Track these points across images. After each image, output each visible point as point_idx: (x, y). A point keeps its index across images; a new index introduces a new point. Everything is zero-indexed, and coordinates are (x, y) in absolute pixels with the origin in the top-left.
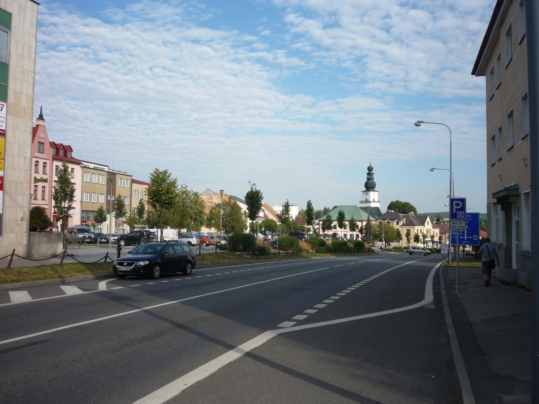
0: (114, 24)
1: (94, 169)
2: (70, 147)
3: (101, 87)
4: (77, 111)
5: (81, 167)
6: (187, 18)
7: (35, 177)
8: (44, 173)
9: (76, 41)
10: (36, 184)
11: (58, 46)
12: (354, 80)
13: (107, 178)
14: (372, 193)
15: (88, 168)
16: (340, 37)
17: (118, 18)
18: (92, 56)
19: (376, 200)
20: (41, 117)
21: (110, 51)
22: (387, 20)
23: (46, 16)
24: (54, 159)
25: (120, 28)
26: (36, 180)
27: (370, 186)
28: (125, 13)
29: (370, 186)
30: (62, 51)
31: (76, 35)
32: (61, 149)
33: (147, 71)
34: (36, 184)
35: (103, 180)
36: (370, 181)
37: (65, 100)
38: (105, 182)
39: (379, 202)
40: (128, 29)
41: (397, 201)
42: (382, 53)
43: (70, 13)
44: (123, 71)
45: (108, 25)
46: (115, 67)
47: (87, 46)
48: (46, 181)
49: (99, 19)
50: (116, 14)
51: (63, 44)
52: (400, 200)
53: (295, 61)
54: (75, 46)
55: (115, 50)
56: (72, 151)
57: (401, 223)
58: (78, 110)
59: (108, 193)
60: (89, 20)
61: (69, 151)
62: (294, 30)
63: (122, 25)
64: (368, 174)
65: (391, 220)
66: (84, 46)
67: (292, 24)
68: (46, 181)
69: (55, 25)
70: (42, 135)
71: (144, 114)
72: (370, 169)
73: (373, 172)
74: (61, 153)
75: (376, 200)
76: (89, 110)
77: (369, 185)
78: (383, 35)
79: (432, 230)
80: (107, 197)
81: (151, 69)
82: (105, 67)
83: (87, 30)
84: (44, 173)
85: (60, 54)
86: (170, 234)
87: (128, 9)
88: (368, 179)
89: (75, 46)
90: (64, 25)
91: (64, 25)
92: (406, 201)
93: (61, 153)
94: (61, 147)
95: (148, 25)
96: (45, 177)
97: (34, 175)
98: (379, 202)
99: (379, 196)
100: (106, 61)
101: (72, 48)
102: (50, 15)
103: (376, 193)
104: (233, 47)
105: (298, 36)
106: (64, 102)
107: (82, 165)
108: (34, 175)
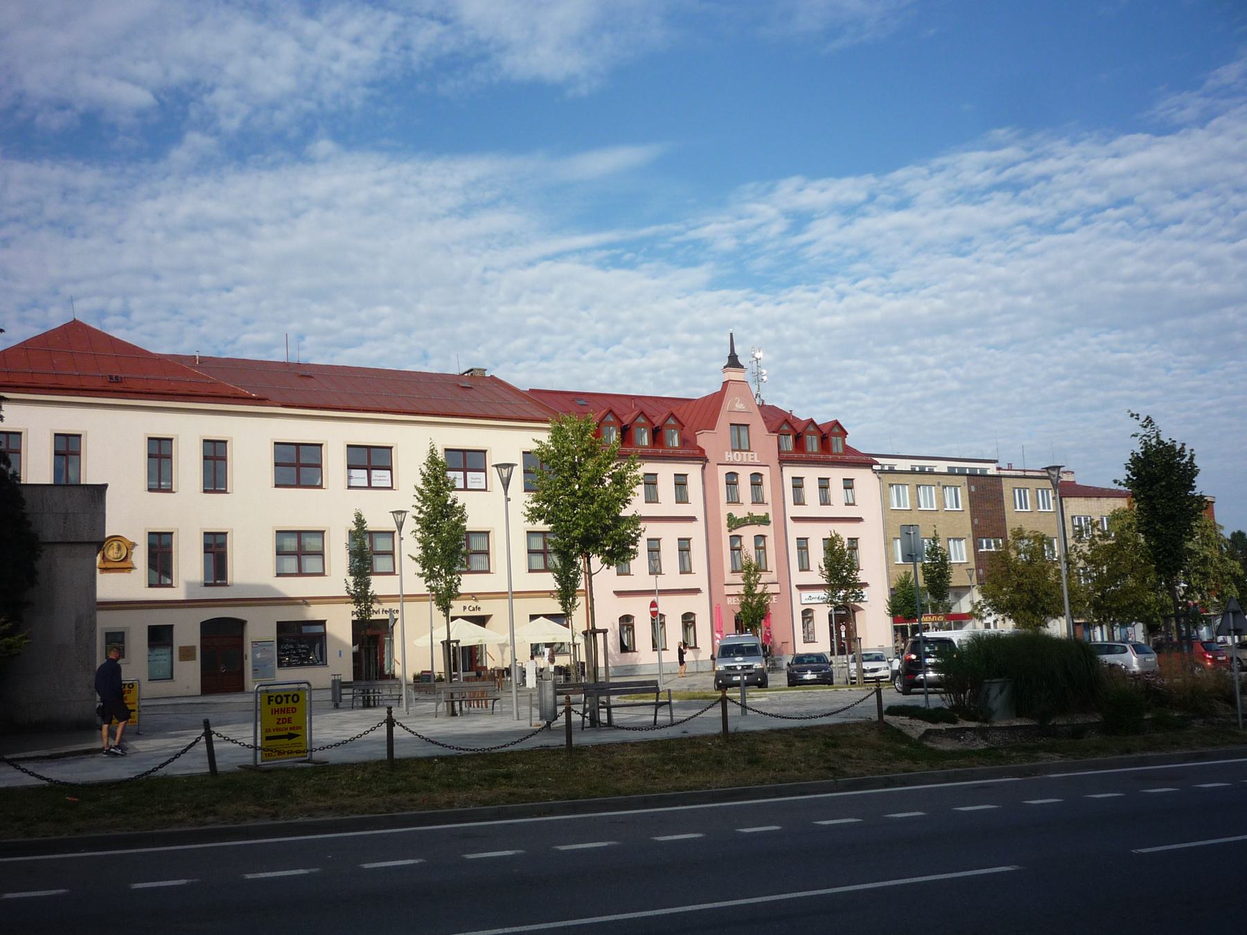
0: (1182, 132)
1: (913, 472)
2: (837, 423)
3: (1176, 285)
4: (1125, 355)
5: (875, 471)
7: (730, 515)
8: (758, 500)
9: (1098, 198)
10: (735, 532)
11: (1062, 221)
13: (970, 493)
15: (931, 473)
17: (1190, 113)
18: (1142, 221)
20: (733, 362)
21: (1185, 196)
23: (1024, 165)
24: (784, 460)
25: (1199, 135)
26: (734, 523)
28: (1206, 96)
30: (1071, 230)
32: (811, 434)
34: (735, 532)
35: (957, 500)
37: (1095, 336)
38: (964, 503)
40: (1220, 131)
43: (1074, 142)
44: (1225, 233)
45: (1168, 138)
46: (1202, 230)
47: (1128, 201)
48: (764, 521)
49: (1145, 130)
50: (1182, 107)
51: (1073, 213)
54: (1100, 209)
55: (1197, 190)
56: (844, 433)
58: (1129, 351)
59: (978, 534)
60: (1122, 142)
61: (836, 435)
63: (1202, 127)
66: (1118, 204)
68: (764, 521)
69: (1046, 178)
70: (739, 406)
74: (813, 444)
76: (1155, 346)
80: (977, 546)
82: (1180, 238)
84: (758, 500)
85: (1069, 236)
86: (758, 665)
89: (1100, 209)
90: (1067, 171)
91: (1067, 171)
93: (813, 444)
94: (811, 429)
96: (759, 511)
97: (725, 509)
101: (1094, 217)
102: (1035, 158)
106: (1093, 340)
107: (875, 467)
108: (725, 509)
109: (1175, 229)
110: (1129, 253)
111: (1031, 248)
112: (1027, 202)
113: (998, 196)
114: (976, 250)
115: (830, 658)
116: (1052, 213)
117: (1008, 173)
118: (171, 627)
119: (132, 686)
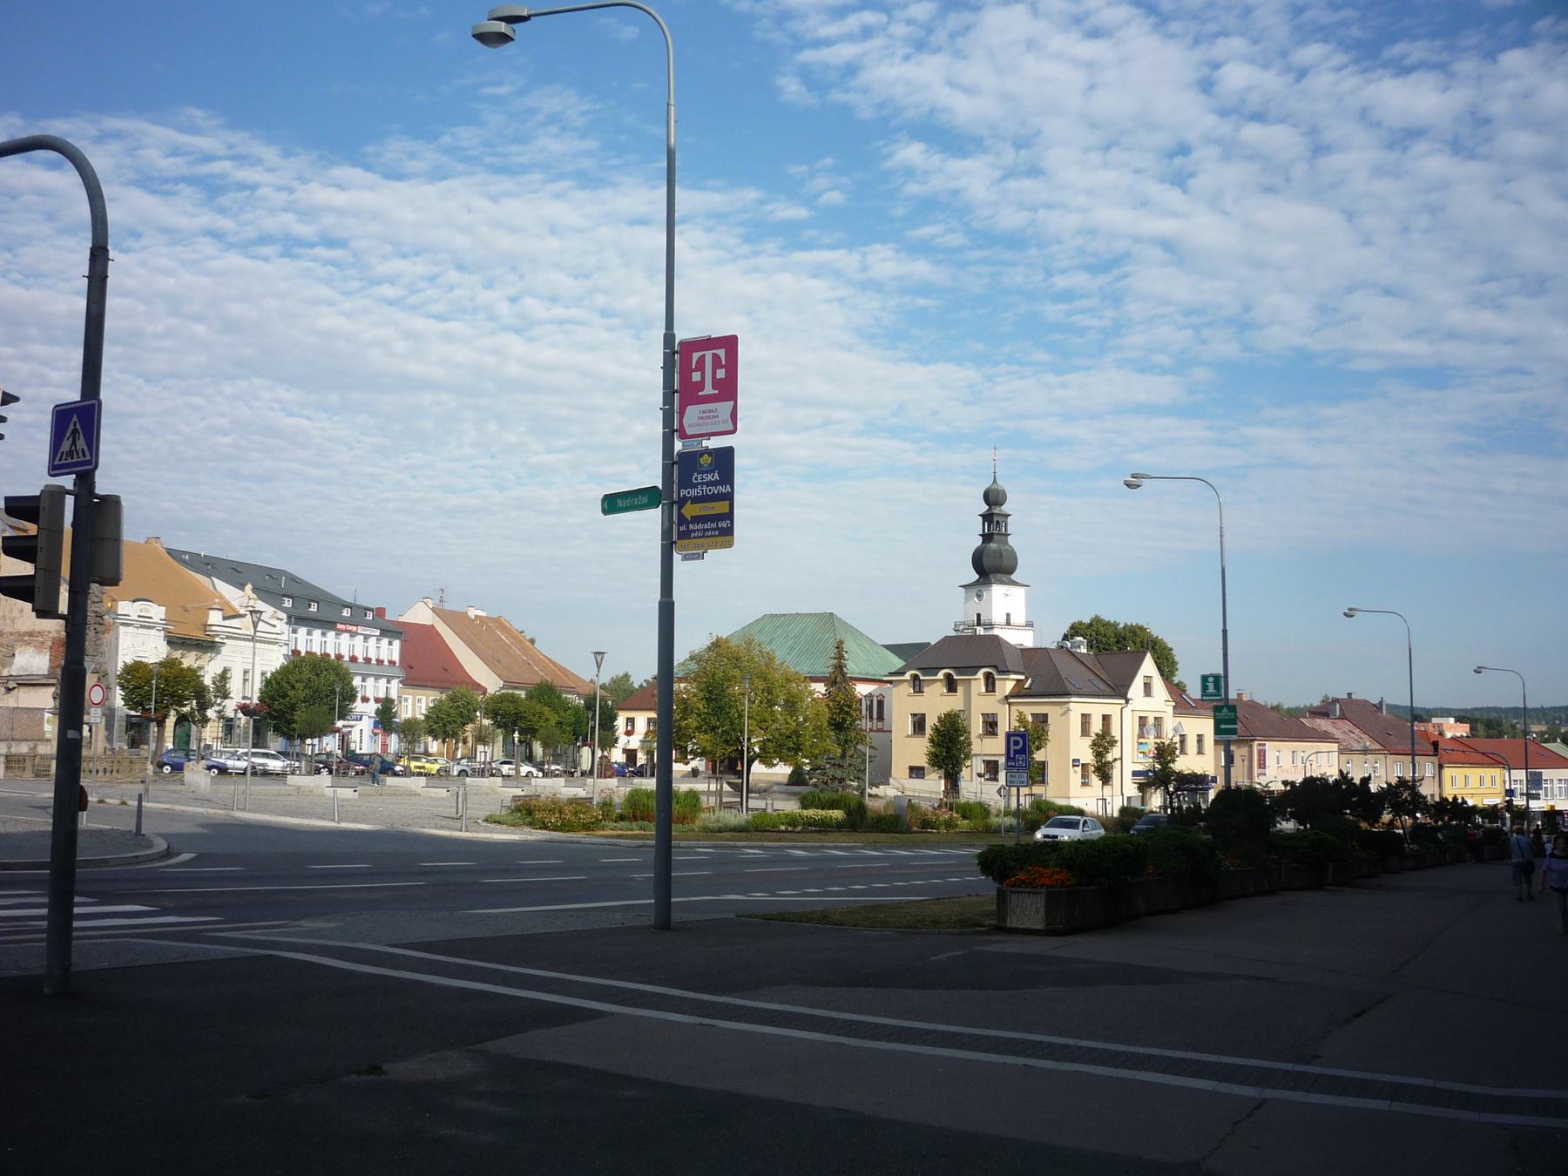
4: (303, 421)
6: (614, 162)
9: (303, 230)
12: (1093, 322)
14: (997, 591)
16: (1049, 206)
19: (1019, 618)
21: (404, 256)
22: (1179, 161)
25: (431, 191)
27: (992, 565)
29: (992, 565)
30: (266, 259)
31: (307, 213)
33: (504, 309)
36: (993, 545)
39: (1029, 625)
41: (1141, 628)
42: (1167, 245)
52: (1107, 617)
53: (921, 268)
57: (1006, 685)
58: (309, 418)
62: (913, 188)
64: (987, 518)
65: (961, 670)
66: (330, 242)
67: (909, 172)
69: (253, 187)
71: (492, 427)
72: (993, 498)
73: (1005, 508)
75: (1019, 618)
77: (986, 562)
78: (1173, 197)
79: (1170, 722)
81: (513, 300)
83: (340, 199)
85: (259, 265)
87: (446, 139)
88: (987, 538)
92: (1133, 620)
95: (506, 184)
98: (1029, 625)
99: (1030, 604)
100: (392, 281)
103: (1018, 593)
104: (747, 239)
105: (927, 208)
109: (387, 291)
110: (331, 304)
111: (214, 265)
112: (222, 211)
113: (186, 190)
114: (144, 248)
115: (1094, 737)
116: (250, 233)
117: (206, 169)
118: (7, 499)
119: (749, 643)
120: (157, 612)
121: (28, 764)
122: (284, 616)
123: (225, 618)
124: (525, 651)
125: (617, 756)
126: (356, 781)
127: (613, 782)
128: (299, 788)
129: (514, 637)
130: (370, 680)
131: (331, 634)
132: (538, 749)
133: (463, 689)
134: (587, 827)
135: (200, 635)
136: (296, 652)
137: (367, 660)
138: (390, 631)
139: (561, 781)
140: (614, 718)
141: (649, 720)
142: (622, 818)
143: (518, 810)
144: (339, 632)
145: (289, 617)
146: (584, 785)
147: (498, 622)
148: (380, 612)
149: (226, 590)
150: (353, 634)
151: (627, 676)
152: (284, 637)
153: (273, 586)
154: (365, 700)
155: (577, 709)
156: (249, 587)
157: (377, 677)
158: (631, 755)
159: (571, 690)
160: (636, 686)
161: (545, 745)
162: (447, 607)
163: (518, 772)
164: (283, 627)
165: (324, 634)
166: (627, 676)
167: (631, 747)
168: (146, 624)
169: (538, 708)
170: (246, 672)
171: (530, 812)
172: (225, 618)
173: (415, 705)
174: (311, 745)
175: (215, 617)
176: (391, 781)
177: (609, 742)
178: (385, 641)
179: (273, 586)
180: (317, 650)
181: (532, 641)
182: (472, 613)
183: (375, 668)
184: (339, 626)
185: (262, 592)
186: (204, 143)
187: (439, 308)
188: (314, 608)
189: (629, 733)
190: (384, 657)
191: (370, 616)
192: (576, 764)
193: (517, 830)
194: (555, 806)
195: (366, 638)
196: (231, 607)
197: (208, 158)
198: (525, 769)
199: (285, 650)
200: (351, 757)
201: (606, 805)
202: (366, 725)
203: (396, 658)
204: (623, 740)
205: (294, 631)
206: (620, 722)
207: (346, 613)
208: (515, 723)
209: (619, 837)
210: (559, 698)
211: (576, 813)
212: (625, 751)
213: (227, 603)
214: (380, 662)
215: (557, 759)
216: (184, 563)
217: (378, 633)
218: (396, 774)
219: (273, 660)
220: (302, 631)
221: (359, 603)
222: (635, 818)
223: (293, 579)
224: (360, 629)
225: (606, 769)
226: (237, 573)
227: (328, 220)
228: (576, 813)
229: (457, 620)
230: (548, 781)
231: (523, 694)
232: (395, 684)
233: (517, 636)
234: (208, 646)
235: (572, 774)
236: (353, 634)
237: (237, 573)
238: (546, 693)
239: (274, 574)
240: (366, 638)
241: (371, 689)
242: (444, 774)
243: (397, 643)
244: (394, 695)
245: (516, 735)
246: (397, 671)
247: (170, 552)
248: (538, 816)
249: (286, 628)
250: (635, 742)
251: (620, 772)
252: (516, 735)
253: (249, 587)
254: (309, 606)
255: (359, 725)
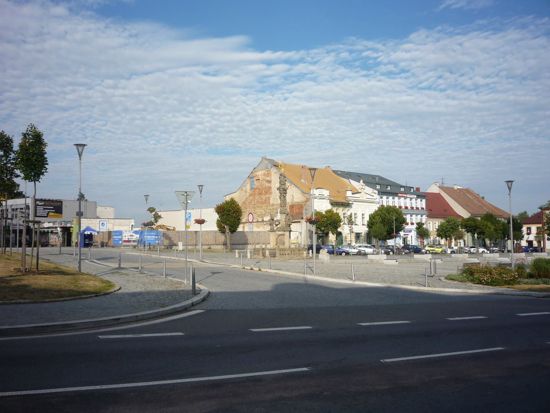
66: (403, 71)
120: (326, 193)
121: (261, 252)
122: (377, 192)
123: (353, 194)
124: (479, 201)
125: (524, 243)
126: (405, 256)
127: (523, 255)
128: (372, 260)
129: (474, 196)
130: (414, 216)
131: (396, 198)
132: (488, 242)
133: (452, 218)
134: (508, 283)
135: (344, 201)
136: (382, 206)
137: (412, 208)
138: (420, 196)
139: (497, 255)
140: (522, 227)
141: (538, 228)
142: (531, 276)
143: (465, 272)
144: (400, 197)
145: (379, 192)
146: (508, 256)
147: (468, 191)
148: (418, 189)
149: (354, 183)
150: (405, 198)
151: (525, 213)
152: (377, 200)
153: (371, 181)
154: (412, 224)
155: (504, 224)
156: (362, 181)
157: (417, 215)
158: (530, 243)
159: (500, 216)
160: (530, 216)
161: (490, 240)
162: (445, 185)
163: (478, 251)
164: (377, 196)
165: (393, 198)
166: (525, 213)
167: (530, 239)
168: (322, 198)
169: (485, 223)
170: (363, 215)
171: (472, 273)
172: (353, 194)
173: (432, 225)
174: (390, 242)
175: (349, 194)
176: (416, 256)
177: (519, 236)
178: (419, 200)
179: (371, 181)
180: (391, 204)
181: (483, 198)
182: (456, 187)
183: (415, 211)
184: (399, 195)
185: (367, 183)
186: (359, 47)
187: (442, 87)
188: (389, 188)
189: (529, 234)
190: (419, 206)
191: (412, 191)
192: (505, 247)
193: (463, 285)
194: (487, 270)
195: (411, 199)
196: (356, 190)
197: (361, 52)
198: (481, 250)
199: (378, 205)
200: (406, 246)
201: (520, 267)
202: (414, 234)
203: (424, 206)
204: (526, 237)
205: (381, 198)
206: (524, 229)
207: (402, 189)
208: (475, 230)
209: (530, 290)
210: (495, 219)
211: (500, 274)
212: (527, 241)
213: (355, 188)
214: (417, 208)
215: (496, 245)
216: (339, 175)
217: (416, 197)
218: (422, 253)
219: (373, 208)
220: (385, 197)
221: (408, 186)
222: (539, 276)
223: (382, 178)
224: (408, 196)
225: (518, 249)
226: (357, 177)
227: (402, 64)
228: (500, 274)
229: (449, 191)
230: (492, 255)
231: (479, 218)
232: (424, 217)
233: (476, 196)
234: (346, 205)
235: (503, 252)
236: (405, 198)
237: (357, 177)
238: (490, 217)
239: (374, 177)
240: (411, 199)
241: (412, 220)
242: (444, 253)
243: (424, 201)
244: (424, 222)
245: (476, 235)
246: (425, 212)
247: (334, 171)
248: (476, 276)
249: (378, 197)
250: (532, 237)
251: (526, 250)
252: (476, 235)
253: (362, 181)
254: (386, 187)
255: (411, 234)
